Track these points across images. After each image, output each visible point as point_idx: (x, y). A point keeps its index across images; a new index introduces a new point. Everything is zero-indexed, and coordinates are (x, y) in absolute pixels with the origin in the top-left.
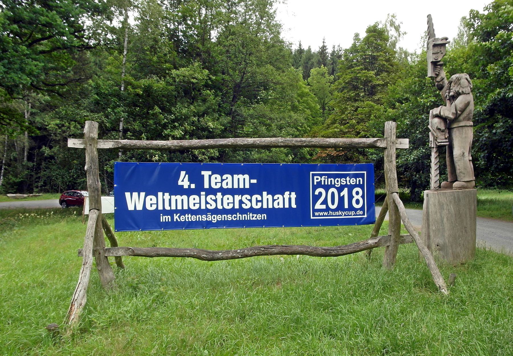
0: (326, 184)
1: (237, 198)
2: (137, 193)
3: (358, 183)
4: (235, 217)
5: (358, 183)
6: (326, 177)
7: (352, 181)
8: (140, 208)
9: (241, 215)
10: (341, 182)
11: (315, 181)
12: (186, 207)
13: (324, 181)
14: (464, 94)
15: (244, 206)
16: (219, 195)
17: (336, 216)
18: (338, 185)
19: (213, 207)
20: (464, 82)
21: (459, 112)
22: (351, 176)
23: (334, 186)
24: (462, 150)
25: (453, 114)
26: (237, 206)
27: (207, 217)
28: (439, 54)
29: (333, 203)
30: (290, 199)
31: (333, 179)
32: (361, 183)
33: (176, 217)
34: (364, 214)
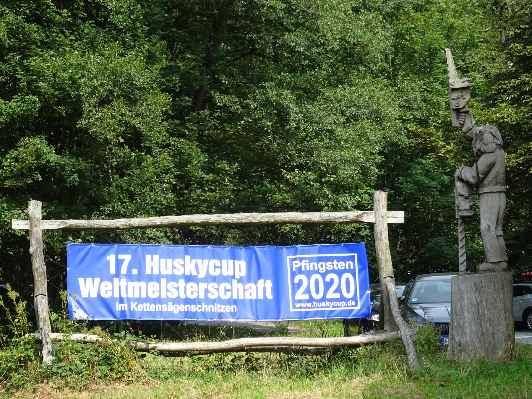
0: (308, 269)
1: (203, 286)
2: (91, 279)
3: (347, 268)
4: (199, 308)
5: (347, 268)
6: (307, 261)
7: (341, 265)
8: (94, 295)
9: (206, 306)
10: (326, 266)
11: (294, 267)
12: (144, 296)
13: (305, 266)
14: (487, 153)
15: (210, 296)
16: (182, 282)
17: (322, 307)
18: (323, 270)
19: (175, 296)
20: (487, 137)
21: (480, 176)
22: (339, 259)
23: (317, 272)
24: (488, 222)
25: (474, 177)
26: (202, 296)
27: (167, 307)
28: (460, 100)
29: (348, 291)
30: (264, 288)
31: (315, 264)
32: (352, 268)
33: (133, 306)
34: (356, 305)
